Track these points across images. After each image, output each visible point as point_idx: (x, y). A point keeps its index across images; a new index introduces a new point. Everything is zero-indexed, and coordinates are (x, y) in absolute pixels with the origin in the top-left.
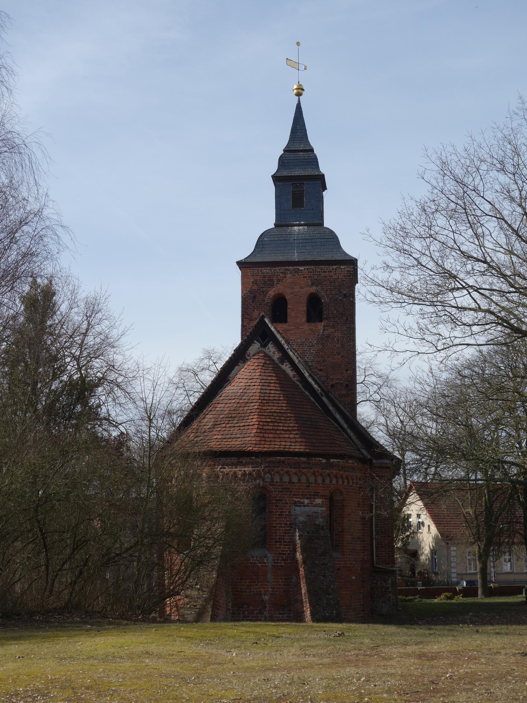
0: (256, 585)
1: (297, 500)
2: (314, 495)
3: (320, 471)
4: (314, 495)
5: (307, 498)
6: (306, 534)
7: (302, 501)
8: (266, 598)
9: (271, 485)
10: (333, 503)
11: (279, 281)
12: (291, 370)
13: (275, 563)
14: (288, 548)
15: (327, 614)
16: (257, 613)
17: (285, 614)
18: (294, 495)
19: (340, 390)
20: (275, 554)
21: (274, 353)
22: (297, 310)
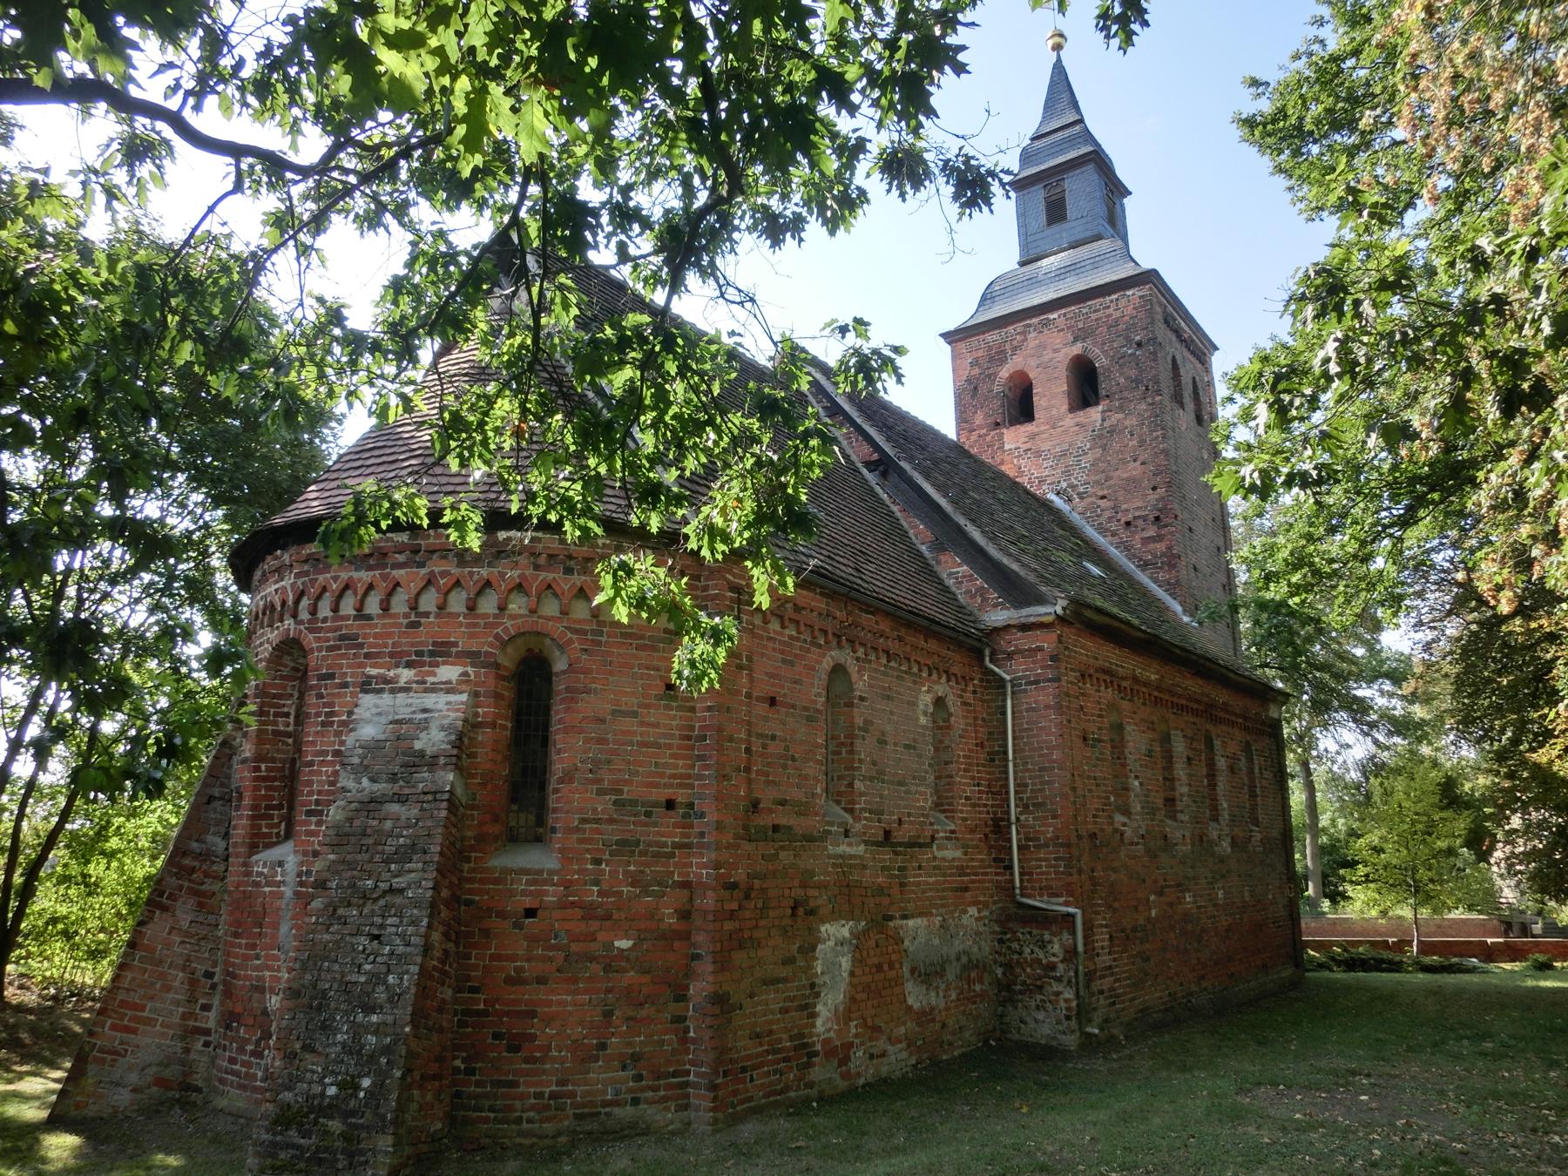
1: (374, 672)
2: (432, 654)
3: (455, 571)
4: (432, 654)
5: (409, 665)
7: (391, 673)
8: (274, 1002)
9: (311, 630)
11: (1015, 349)
15: (332, 1091)
18: (367, 656)
22: (1051, 395)
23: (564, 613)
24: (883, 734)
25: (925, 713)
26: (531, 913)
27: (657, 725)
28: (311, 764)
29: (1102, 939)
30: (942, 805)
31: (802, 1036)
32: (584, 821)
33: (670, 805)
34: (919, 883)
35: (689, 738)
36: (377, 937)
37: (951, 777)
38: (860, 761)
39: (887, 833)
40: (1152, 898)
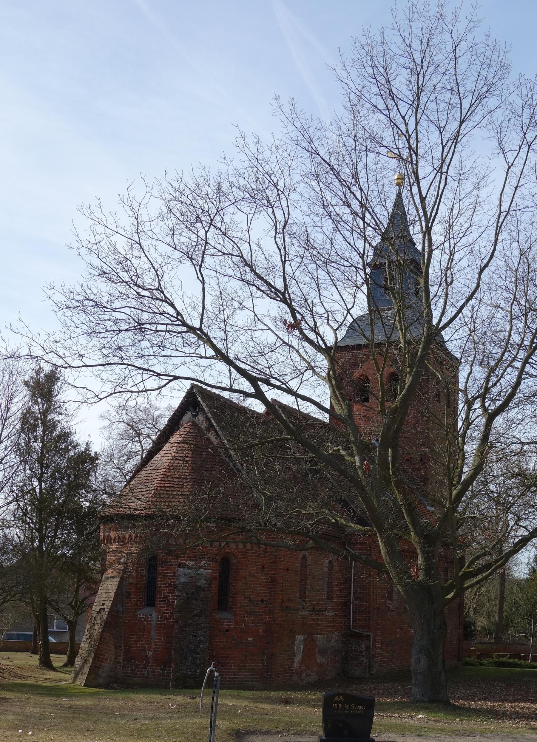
0: (142, 641)
1: (182, 562)
5: (193, 560)
6: (185, 594)
7: (187, 563)
8: (150, 654)
10: (225, 566)
12: (216, 438)
13: (159, 621)
14: (171, 608)
15: (190, 673)
16: (142, 668)
17: (165, 670)
19: (414, 464)
20: (160, 612)
21: (203, 422)
23: (237, 547)
24: (314, 576)
25: (326, 567)
26: (227, 630)
27: (259, 579)
28: (161, 587)
29: (378, 644)
30: (329, 598)
31: (291, 667)
32: (241, 606)
33: (262, 601)
34: (321, 624)
35: (267, 582)
36: (195, 636)
37: (332, 587)
38: (308, 585)
39: (314, 607)
40: (398, 630)
